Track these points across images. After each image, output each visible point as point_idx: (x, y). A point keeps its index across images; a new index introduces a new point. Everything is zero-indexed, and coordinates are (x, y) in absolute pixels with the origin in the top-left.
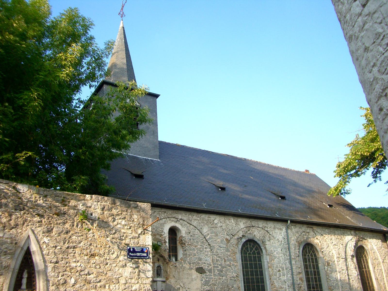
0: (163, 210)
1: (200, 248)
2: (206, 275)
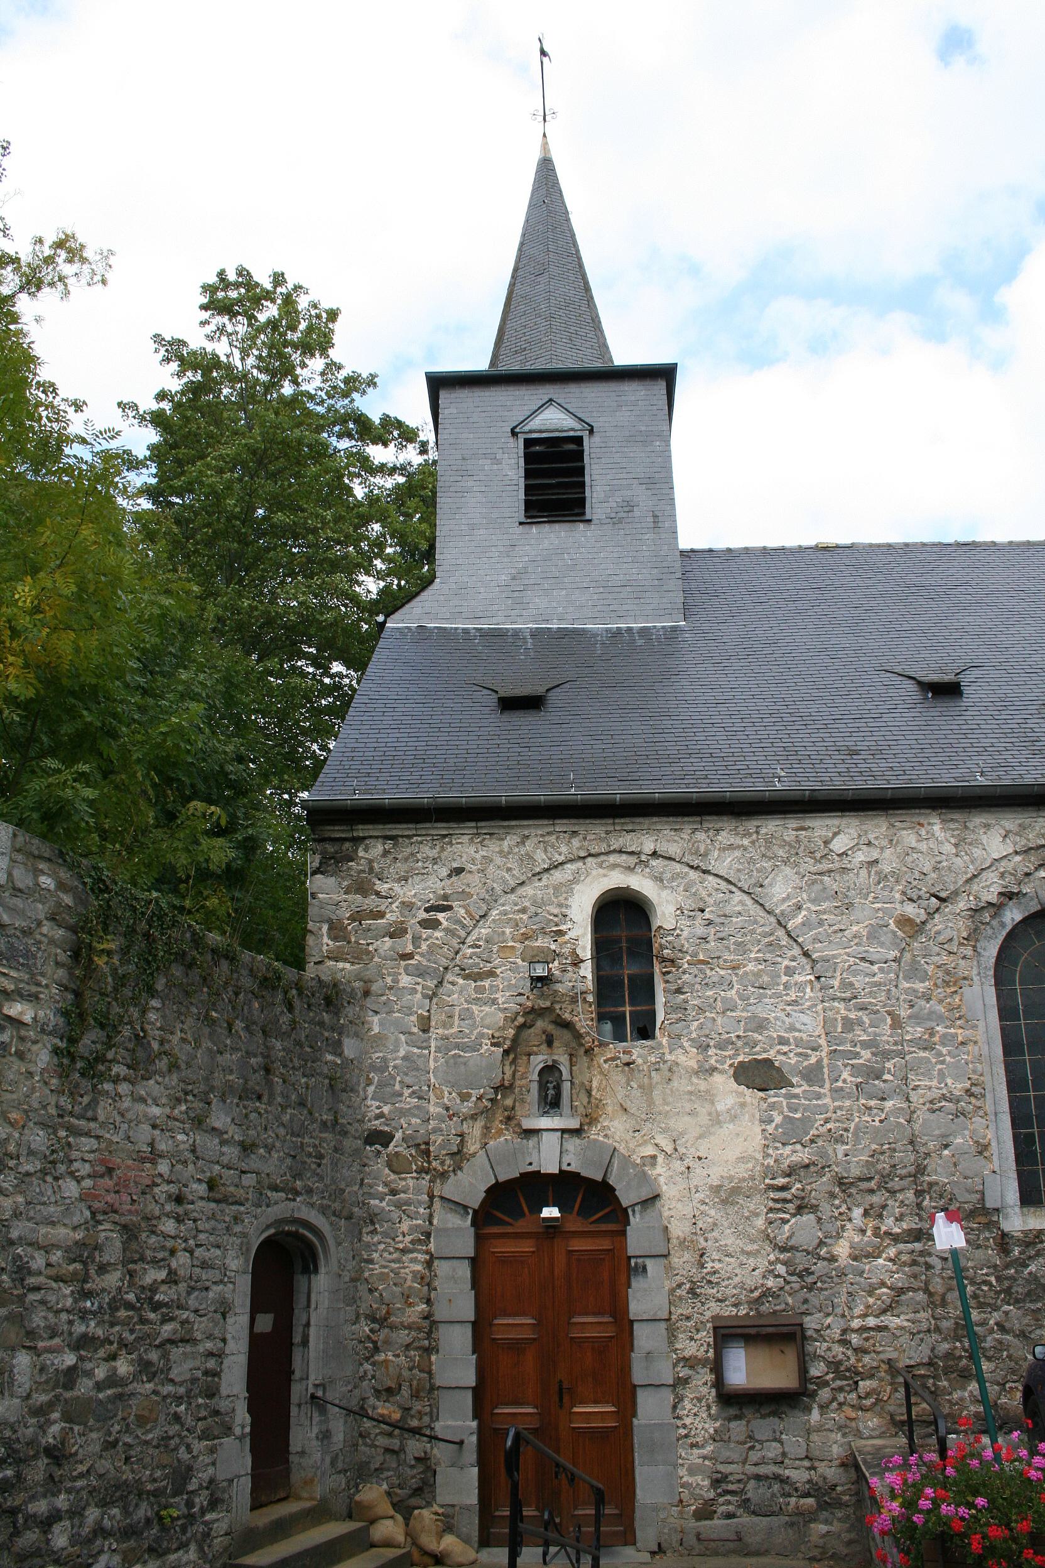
0: (562, 825)
1: (758, 975)
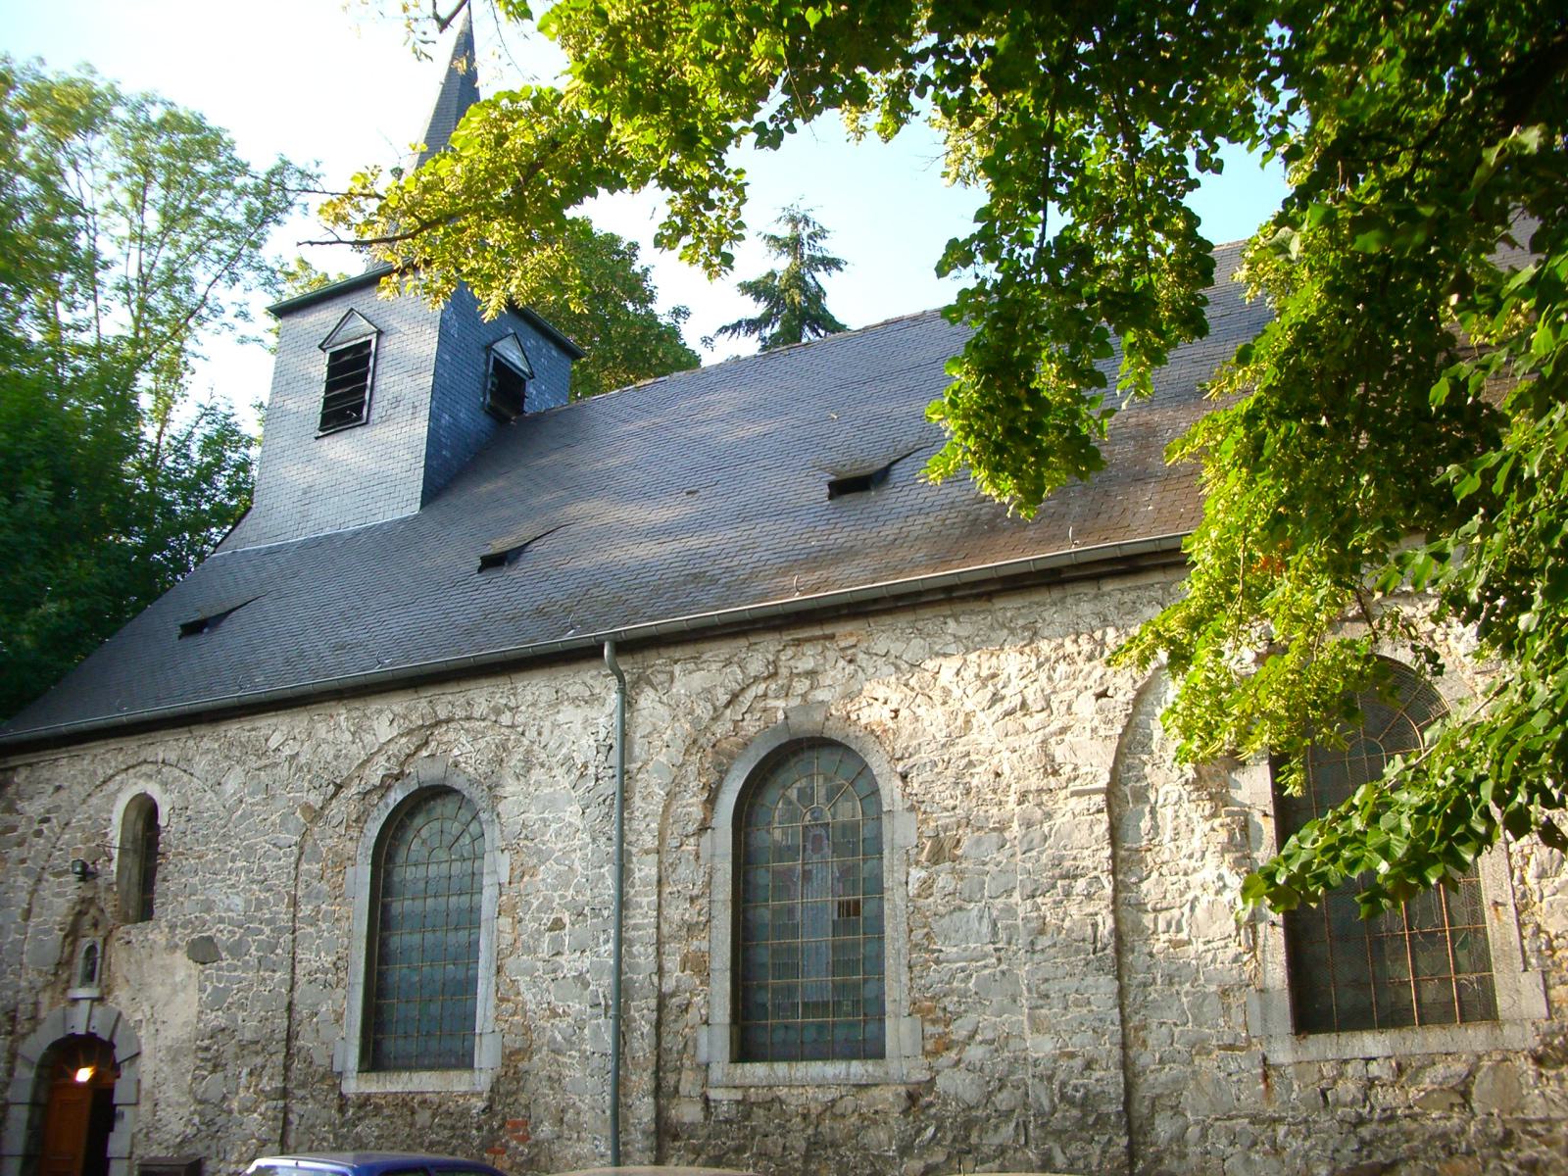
0: (113, 744)
1: (213, 863)
2: (220, 969)
